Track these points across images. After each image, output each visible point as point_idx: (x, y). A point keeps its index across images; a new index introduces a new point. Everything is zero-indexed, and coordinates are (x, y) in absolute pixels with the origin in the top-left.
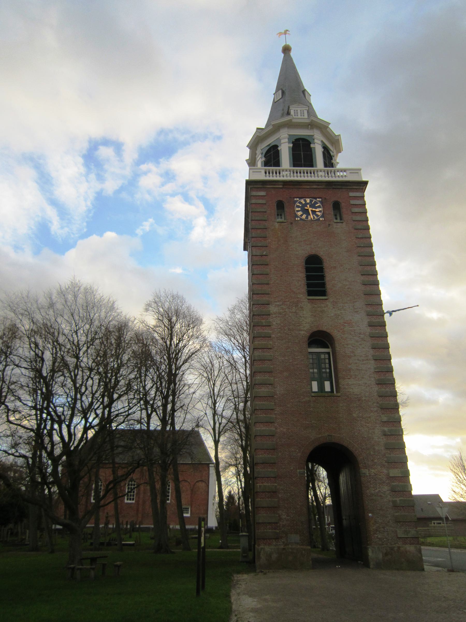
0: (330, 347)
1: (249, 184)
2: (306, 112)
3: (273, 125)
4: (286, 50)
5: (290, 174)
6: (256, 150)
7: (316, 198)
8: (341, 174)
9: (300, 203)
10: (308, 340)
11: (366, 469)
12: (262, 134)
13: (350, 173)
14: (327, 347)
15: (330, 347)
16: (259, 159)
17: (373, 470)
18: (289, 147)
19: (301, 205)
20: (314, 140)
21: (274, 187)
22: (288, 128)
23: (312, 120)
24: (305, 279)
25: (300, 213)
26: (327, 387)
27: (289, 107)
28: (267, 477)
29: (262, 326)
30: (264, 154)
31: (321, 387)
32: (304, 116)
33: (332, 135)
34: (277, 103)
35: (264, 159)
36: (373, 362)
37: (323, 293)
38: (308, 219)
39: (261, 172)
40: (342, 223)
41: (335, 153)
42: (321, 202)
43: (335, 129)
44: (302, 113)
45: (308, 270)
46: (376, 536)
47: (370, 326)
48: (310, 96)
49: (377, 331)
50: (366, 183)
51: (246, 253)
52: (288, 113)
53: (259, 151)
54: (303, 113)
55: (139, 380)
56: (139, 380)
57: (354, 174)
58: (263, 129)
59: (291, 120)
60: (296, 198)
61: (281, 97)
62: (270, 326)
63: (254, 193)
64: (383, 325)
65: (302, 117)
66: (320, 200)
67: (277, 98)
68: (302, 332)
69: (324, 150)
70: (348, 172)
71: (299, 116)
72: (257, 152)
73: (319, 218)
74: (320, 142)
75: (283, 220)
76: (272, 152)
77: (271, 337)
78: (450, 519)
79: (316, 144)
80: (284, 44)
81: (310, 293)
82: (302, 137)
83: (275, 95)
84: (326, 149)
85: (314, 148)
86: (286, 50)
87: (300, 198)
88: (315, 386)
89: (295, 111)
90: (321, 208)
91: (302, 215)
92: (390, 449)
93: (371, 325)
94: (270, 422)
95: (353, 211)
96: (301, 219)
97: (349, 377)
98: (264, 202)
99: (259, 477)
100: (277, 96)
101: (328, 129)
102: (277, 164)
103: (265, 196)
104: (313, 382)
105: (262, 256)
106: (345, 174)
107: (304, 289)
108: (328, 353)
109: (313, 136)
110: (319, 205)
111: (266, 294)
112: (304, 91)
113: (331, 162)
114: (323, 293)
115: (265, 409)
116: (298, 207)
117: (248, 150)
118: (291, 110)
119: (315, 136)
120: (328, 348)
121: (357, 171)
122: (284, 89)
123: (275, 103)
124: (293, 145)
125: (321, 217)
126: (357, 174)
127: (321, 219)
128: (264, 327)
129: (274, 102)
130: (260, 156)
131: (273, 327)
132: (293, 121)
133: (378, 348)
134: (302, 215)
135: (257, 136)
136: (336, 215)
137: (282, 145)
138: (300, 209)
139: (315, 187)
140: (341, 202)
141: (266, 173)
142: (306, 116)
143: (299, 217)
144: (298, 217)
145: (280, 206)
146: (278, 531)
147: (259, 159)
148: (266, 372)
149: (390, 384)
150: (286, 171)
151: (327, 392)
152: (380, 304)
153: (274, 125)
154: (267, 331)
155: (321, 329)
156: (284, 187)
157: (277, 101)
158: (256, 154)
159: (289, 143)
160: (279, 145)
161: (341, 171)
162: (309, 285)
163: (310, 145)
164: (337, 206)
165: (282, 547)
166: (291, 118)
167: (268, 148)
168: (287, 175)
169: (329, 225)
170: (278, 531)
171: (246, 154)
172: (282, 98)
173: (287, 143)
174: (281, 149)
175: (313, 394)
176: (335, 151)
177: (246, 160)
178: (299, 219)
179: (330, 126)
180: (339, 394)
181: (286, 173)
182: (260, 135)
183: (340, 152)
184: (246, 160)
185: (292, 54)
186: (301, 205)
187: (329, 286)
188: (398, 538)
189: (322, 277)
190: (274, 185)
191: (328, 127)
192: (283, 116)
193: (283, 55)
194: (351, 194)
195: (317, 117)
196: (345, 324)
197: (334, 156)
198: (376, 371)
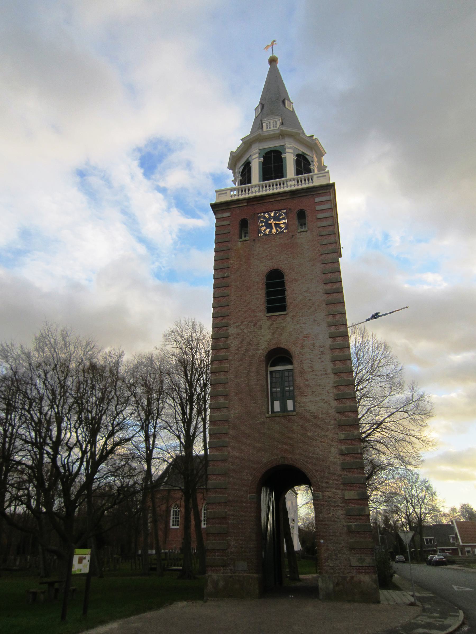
7: (280, 210)
9: (264, 218)
13: (317, 177)
17: (327, 493)
35: (262, 160)
36: (332, 376)
45: (268, 285)
46: (328, 564)
49: (338, 342)
60: (260, 213)
66: (285, 211)
68: (260, 352)
73: (283, 231)
77: (228, 359)
81: (269, 310)
85: (285, 158)
87: (264, 213)
91: (265, 230)
96: (265, 235)
97: (306, 394)
107: (263, 308)
110: (283, 216)
111: (225, 316)
114: (283, 308)
116: (262, 222)
125: (285, 229)
127: (285, 231)
128: (222, 351)
131: (231, 349)
134: (265, 230)
138: (263, 224)
139: (279, 199)
144: (261, 232)
146: (226, 558)
155: (279, 346)
156: (249, 204)
165: (230, 574)
170: (226, 558)
178: (262, 234)
186: (264, 220)
190: (238, 204)
194: (317, 200)
196: (304, 339)
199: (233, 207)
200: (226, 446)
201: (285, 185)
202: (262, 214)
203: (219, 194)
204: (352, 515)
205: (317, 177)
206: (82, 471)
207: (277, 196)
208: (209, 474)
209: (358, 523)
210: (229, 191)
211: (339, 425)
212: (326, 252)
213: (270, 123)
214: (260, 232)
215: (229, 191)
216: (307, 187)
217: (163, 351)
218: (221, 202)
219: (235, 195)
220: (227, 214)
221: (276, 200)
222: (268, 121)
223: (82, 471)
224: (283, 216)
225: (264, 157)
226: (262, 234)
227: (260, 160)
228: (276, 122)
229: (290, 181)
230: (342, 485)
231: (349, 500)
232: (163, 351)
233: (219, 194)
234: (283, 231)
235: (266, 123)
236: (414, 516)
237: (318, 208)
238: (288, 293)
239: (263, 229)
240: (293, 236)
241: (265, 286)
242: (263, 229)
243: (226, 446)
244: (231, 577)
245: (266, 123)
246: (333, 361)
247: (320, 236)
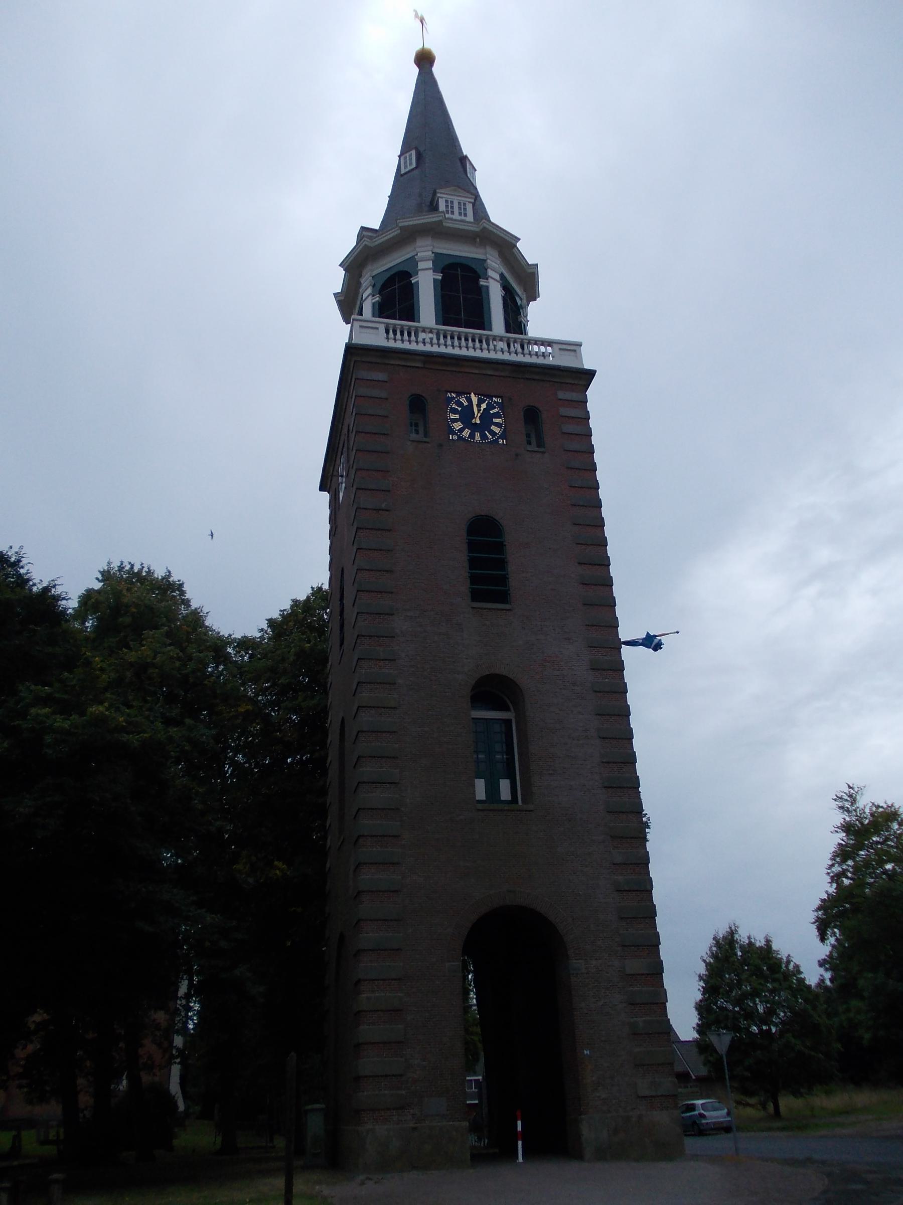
0: (512, 709)
1: (352, 352)
2: (469, 207)
3: (401, 228)
4: (425, 60)
5: (438, 339)
6: (360, 276)
7: (490, 397)
8: (543, 349)
9: (459, 404)
10: (472, 690)
11: (581, 959)
12: (377, 243)
14: (504, 708)
15: (512, 709)
17: (594, 962)
18: (435, 280)
19: (459, 409)
20: (486, 270)
21: (409, 364)
23: (484, 228)
24: (466, 564)
25: (458, 426)
26: (505, 792)
27: (435, 193)
28: (382, 980)
29: (377, 660)
30: (379, 286)
31: (493, 790)
32: (465, 215)
33: (522, 262)
34: (405, 176)
37: (502, 597)
38: (474, 438)
39: (377, 328)
40: (543, 453)
41: (525, 301)
42: (501, 405)
43: (528, 251)
44: (449, 205)
45: (472, 546)
46: (598, 1095)
47: (594, 669)
48: (475, 170)
49: (607, 680)
50: (591, 374)
51: (326, 496)
52: (433, 207)
53: (366, 280)
54: (465, 209)
57: (566, 352)
58: (376, 230)
59: (441, 221)
60: (451, 392)
61: (414, 165)
62: (395, 660)
63: (364, 374)
64: (619, 667)
65: (463, 218)
66: (499, 400)
67: (406, 167)
69: (505, 294)
70: (556, 347)
71: (456, 216)
72: (362, 280)
73: (497, 440)
74: (498, 277)
75: (420, 437)
76: (396, 286)
77: (395, 683)
78: (694, 1077)
79: (490, 280)
80: (419, 47)
81: (476, 596)
83: (402, 158)
84: (508, 290)
85: (487, 287)
86: (425, 60)
87: (459, 394)
88: (480, 789)
89: (447, 201)
90: (501, 418)
91: (461, 430)
92: (628, 918)
93: (595, 668)
94: (391, 863)
95: (565, 430)
96: (460, 438)
97: (551, 772)
98: (384, 395)
99: (366, 980)
100: (405, 162)
101: (515, 250)
102: (410, 312)
103: (386, 382)
104: (477, 781)
105: (378, 510)
106: (549, 349)
107: (464, 588)
108: (508, 722)
109: (485, 260)
110: (496, 410)
111: (385, 592)
112: (464, 159)
113: (517, 319)
114: (502, 597)
115: (380, 836)
116: (454, 411)
117: (341, 273)
118: (440, 200)
119: (488, 261)
120: (507, 709)
121: (573, 348)
122: (421, 149)
123: (402, 175)
124: (442, 277)
125: (501, 437)
126: (573, 353)
127: (501, 441)
128: (381, 663)
129: (400, 176)
130: (369, 291)
133: (608, 715)
134: (461, 430)
136: (528, 436)
137: (419, 272)
138: (457, 416)
139: (489, 372)
140: (541, 409)
141: (387, 332)
142: (470, 218)
143: (456, 434)
144: (454, 433)
145: (417, 405)
146: (404, 1092)
148: (383, 757)
149: (630, 788)
150: (431, 332)
151: (479, 802)
152: (614, 625)
153: (404, 227)
154: (387, 671)
155: (497, 672)
157: (406, 173)
158: (359, 284)
159: (434, 272)
160: (412, 274)
161: (542, 345)
162: (474, 579)
163: (477, 282)
164: (532, 416)
165: (412, 1125)
166: (441, 218)
167: (388, 275)
168: (431, 339)
169: (517, 455)
170: (404, 1092)
171: (337, 280)
172: (416, 168)
173: (432, 271)
175: (480, 806)
176: (524, 297)
177: (334, 294)
178: (455, 437)
179: (518, 245)
180: (531, 807)
181: (431, 335)
182: (372, 245)
184: (334, 294)
185: (437, 70)
186: (459, 409)
187: (513, 583)
188: (639, 1097)
189: (502, 564)
191: (515, 246)
192: (419, 210)
193: (416, 70)
194: (561, 395)
195: (489, 221)
196: (544, 664)
197: (522, 308)
198: (604, 761)
199: (392, 362)
200: (398, 864)
201: (413, 338)
204: (637, 1004)
205: (361, 327)
206: (230, 771)
209: (648, 1018)
211: (611, 837)
212: (581, 503)
213: (452, 202)
216: (498, 360)
218: (377, 346)
219: (544, 355)
220: (381, 376)
221: (481, 372)
222: (450, 198)
223: (230, 771)
224: (496, 410)
225: (380, 292)
226: (455, 437)
227: (374, 301)
229: (424, 331)
230: (619, 948)
234: (497, 440)
235: (444, 199)
236: (740, 1022)
237: (564, 411)
238: (511, 568)
240: (517, 455)
241: (466, 546)
242: (458, 426)
243: (398, 864)
244: (415, 1129)
245: (444, 199)
246: (599, 715)
247: (568, 468)
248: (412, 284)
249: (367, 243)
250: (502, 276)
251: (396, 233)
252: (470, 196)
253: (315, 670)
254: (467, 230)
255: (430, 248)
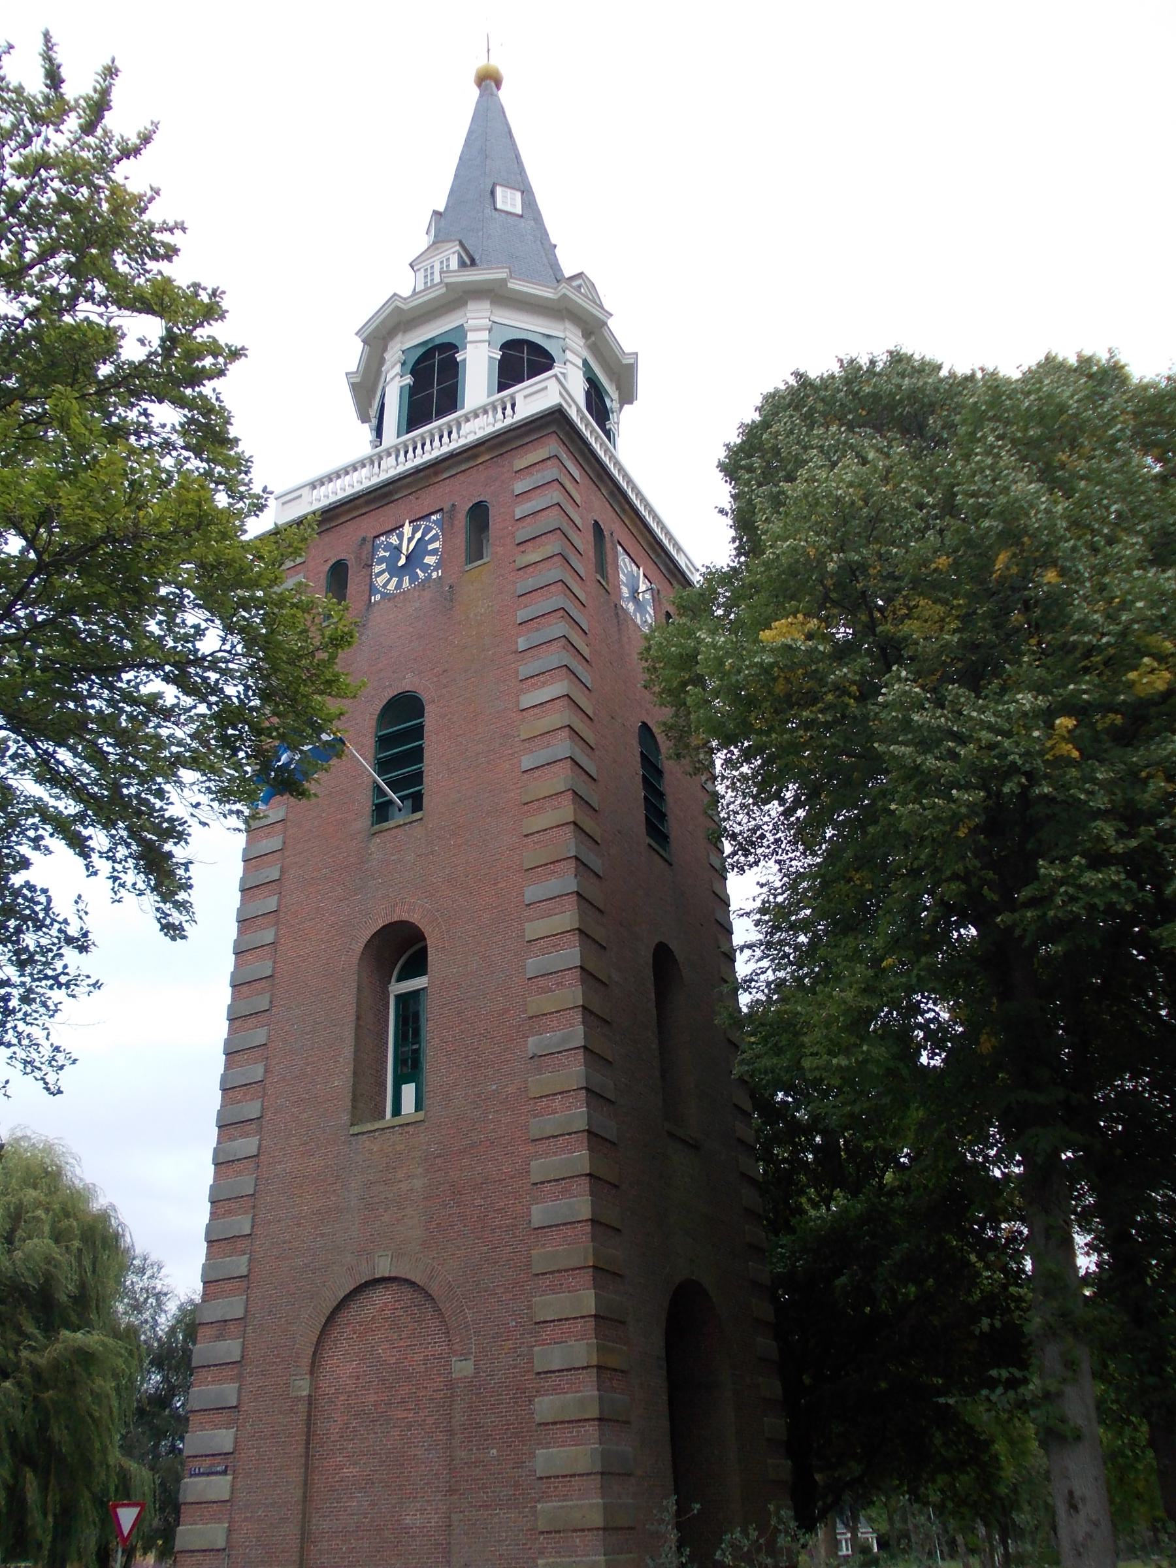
3: (447, 285)
4: (489, 80)
6: (385, 349)
13: (525, 397)
16: (392, 379)
22: (493, 303)
23: (565, 295)
35: (408, 380)
39: (546, 388)
53: (395, 353)
55: (480, 234)
56: (480, 234)
72: (387, 356)
82: (437, 342)
86: (489, 80)
96: (384, 595)
101: (605, 330)
110: (434, 532)
132: (510, 285)
135: (397, 307)
147: (392, 379)
158: (382, 361)
167: (421, 351)
171: (352, 354)
174: (465, 360)
176: (615, 395)
178: (378, 597)
182: (405, 307)
183: (631, 402)
185: (505, 95)
191: (605, 324)
193: (476, 92)
202: (383, 538)
203: (284, 504)
205: (525, 397)
207: (629, 510)
208: (185, 1504)
210: (307, 488)
214: (372, 589)
215: (306, 491)
217: (60, 1442)
224: (434, 532)
225: (413, 372)
226: (378, 597)
227: (402, 384)
228: (448, 259)
231: (148, 309)
232: (60, 1442)
233: (284, 504)
239: (380, 581)
242: (380, 581)
248: (457, 364)
249: (399, 304)
250: (585, 362)
251: (437, 293)
252: (451, 244)
253: (903, 485)
254: (429, 300)
255: (488, 314)
